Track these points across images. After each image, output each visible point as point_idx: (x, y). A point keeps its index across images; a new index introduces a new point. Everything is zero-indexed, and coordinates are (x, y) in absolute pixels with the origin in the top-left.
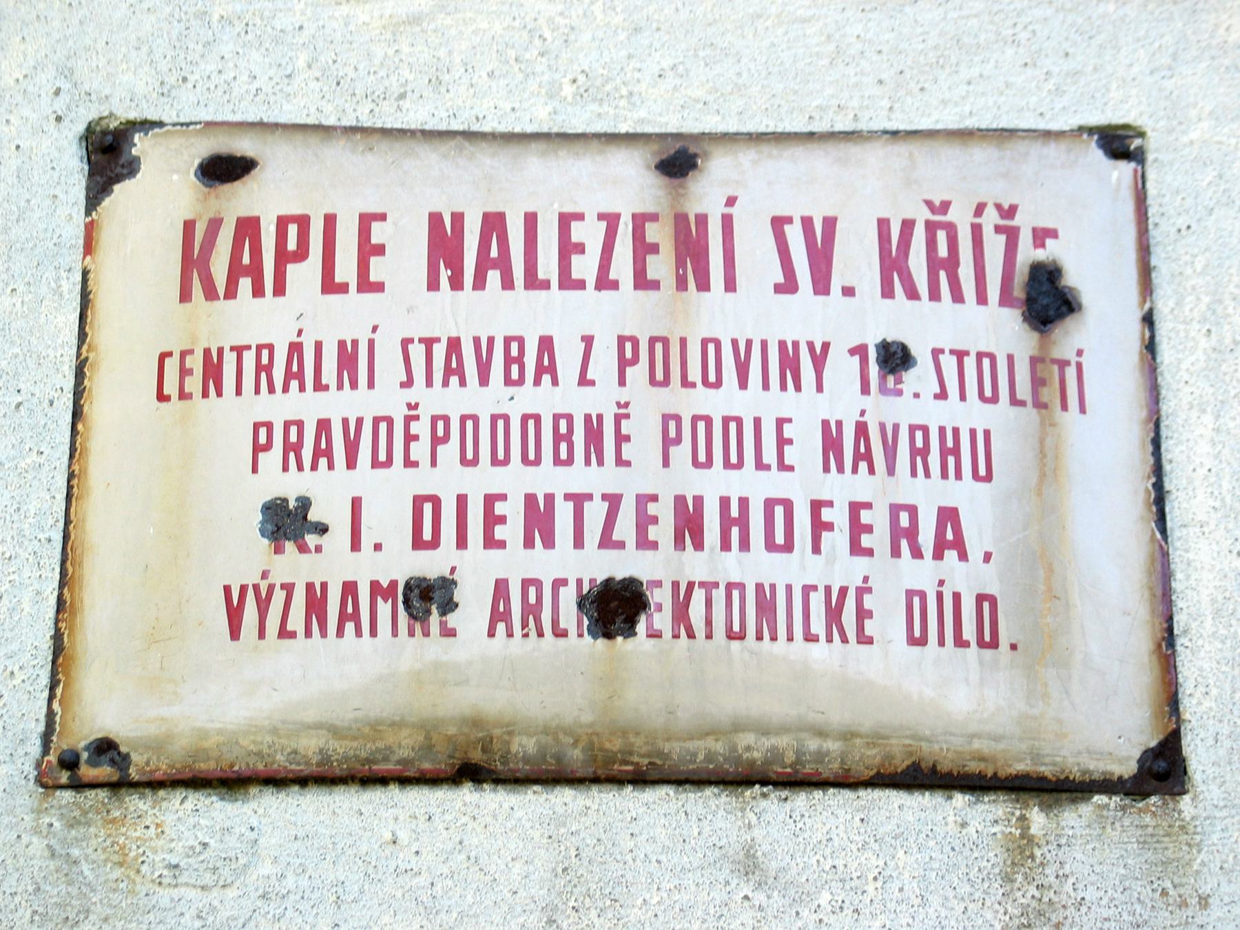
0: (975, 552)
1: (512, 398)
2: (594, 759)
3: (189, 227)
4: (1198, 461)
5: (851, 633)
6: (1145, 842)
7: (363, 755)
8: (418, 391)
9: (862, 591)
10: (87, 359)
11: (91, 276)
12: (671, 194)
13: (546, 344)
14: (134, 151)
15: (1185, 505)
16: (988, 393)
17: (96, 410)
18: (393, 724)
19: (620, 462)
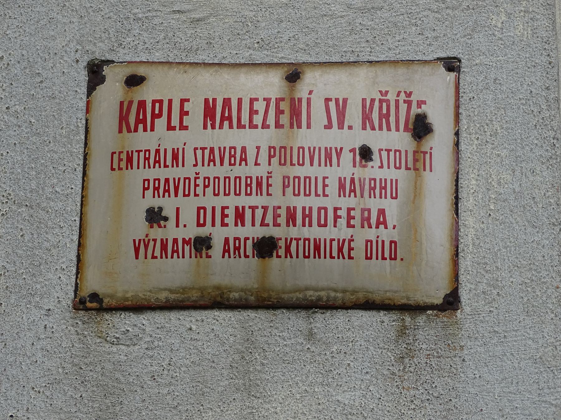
0: (390, 225)
1: (232, 170)
2: (258, 300)
3: (122, 103)
4: (471, 187)
5: (346, 256)
6: (444, 328)
7: (181, 299)
8: (199, 168)
9: (351, 240)
10: (87, 153)
11: (89, 121)
12: (290, 89)
13: (244, 149)
14: (103, 73)
15: (465, 204)
16: (398, 165)
17: (91, 173)
18: (190, 289)
19: (268, 194)
